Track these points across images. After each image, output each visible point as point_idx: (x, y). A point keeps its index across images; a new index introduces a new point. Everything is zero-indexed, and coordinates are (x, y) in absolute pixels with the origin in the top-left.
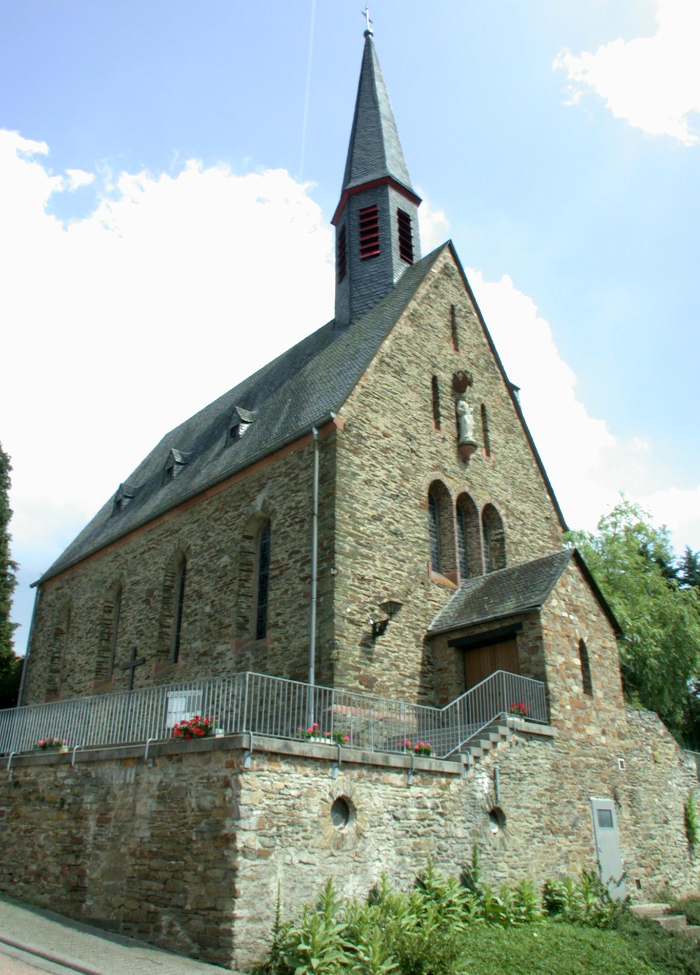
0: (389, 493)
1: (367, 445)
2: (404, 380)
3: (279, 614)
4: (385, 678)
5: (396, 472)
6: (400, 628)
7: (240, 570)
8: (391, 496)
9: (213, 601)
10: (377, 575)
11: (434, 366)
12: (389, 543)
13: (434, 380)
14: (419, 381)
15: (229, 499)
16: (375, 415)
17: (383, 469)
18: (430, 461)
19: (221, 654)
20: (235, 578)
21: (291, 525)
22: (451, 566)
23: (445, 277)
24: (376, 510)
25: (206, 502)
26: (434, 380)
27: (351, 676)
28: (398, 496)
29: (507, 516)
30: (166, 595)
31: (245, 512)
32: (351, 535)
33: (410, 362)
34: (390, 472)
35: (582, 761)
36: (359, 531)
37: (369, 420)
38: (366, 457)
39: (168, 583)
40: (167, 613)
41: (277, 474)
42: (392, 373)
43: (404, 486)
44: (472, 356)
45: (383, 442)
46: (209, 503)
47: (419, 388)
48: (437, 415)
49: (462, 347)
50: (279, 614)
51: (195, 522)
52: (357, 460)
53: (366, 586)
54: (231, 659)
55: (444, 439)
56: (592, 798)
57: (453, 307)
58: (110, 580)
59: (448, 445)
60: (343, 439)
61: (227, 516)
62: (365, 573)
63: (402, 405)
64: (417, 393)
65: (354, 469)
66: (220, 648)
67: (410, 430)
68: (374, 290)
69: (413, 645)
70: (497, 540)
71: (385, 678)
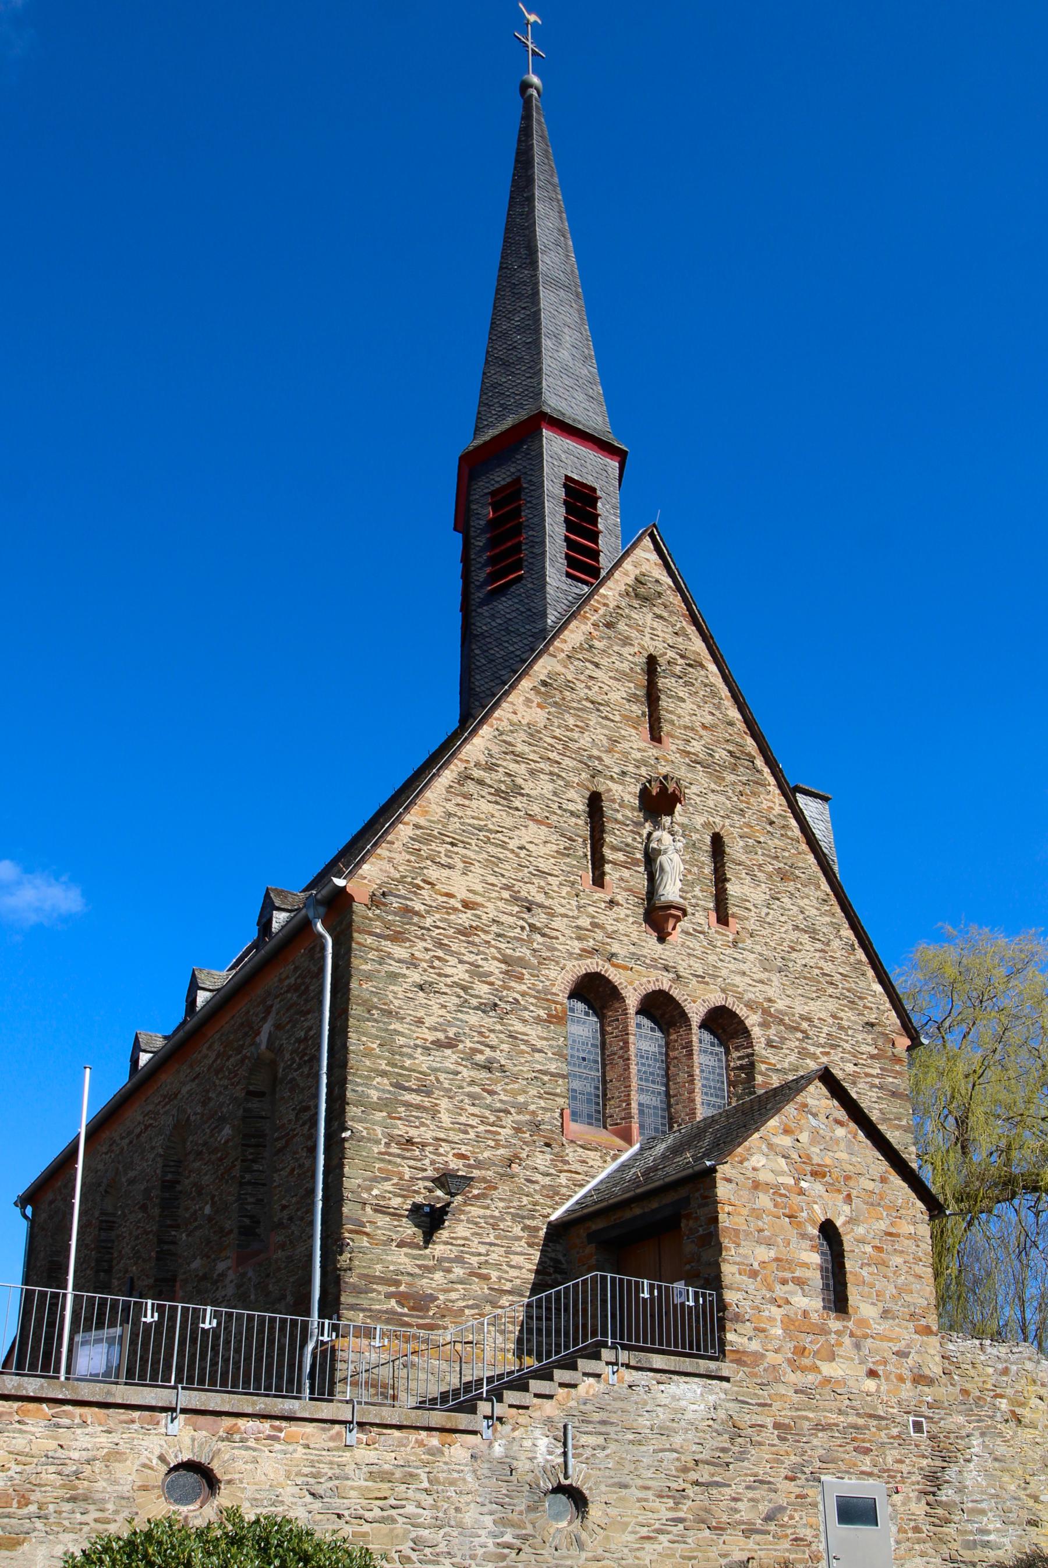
0: (474, 1002)
1: (427, 925)
2: (520, 806)
3: (284, 1207)
4: (453, 1296)
5: (494, 967)
6: (492, 1217)
7: (243, 1145)
8: (481, 1008)
9: (213, 1197)
10: (442, 1136)
11: (595, 774)
12: (472, 1083)
13: (595, 802)
14: (555, 806)
15: (232, 1037)
16: (446, 872)
17: (461, 962)
18: (576, 943)
19: (223, 1275)
20: (236, 1160)
21: (300, 1066)
22: (623, 1114)
23: (636, 603)
24: (445, 1031)
25: (207, 1045)
26: (595, 802)
27: (379, 1293)
28: (496, 1005)
29: (765, 1025)
30: (167, 1195)
31: (248, 1054)
32: (384, 1074)
33: (532, 772)
34: (478, 966)
35: (807, 1418)
36: (402, 1067)
37: (429, 883)
38: (421, 944)
39: (169, 1177)
40: (169, 1222)
41: (285, 989)
42: (490, 798)
43: (509, 988)
44: (696, 747)
45: (465, 918)
46: (210, 1048)
47: (555, 818)
48: (598, 862)
49: (670, 735)
50: (284, 1207)
51: (195, 1078)
52: (400, 952)
53: (417, 1153)
54: (231, 1282)
55: (612, 903)
56: (823, 1478)
57: (652, 662)
58: (105, 1181)
59: (621, 912)
60: (371, 920)
61: (229, 1064)
62: (413, 1132)
63: (512, 851)
64: (549, 826)
65: (394, 967)
66: (221, 1266)
67: (531, 892)
68: (511, 649)
69: (523, 1243)
70: (741, 1068)
71: (453, 1296)
